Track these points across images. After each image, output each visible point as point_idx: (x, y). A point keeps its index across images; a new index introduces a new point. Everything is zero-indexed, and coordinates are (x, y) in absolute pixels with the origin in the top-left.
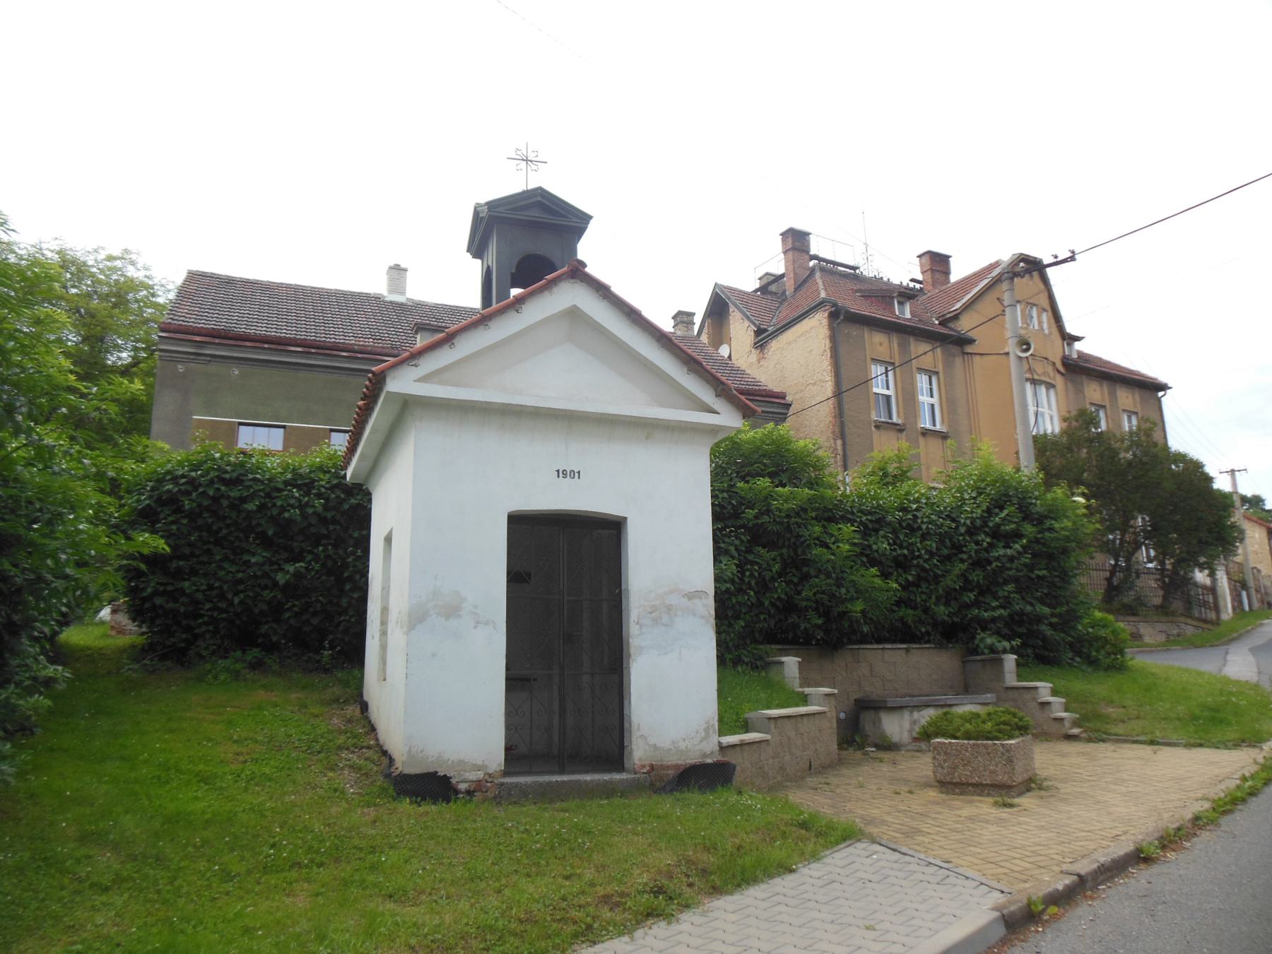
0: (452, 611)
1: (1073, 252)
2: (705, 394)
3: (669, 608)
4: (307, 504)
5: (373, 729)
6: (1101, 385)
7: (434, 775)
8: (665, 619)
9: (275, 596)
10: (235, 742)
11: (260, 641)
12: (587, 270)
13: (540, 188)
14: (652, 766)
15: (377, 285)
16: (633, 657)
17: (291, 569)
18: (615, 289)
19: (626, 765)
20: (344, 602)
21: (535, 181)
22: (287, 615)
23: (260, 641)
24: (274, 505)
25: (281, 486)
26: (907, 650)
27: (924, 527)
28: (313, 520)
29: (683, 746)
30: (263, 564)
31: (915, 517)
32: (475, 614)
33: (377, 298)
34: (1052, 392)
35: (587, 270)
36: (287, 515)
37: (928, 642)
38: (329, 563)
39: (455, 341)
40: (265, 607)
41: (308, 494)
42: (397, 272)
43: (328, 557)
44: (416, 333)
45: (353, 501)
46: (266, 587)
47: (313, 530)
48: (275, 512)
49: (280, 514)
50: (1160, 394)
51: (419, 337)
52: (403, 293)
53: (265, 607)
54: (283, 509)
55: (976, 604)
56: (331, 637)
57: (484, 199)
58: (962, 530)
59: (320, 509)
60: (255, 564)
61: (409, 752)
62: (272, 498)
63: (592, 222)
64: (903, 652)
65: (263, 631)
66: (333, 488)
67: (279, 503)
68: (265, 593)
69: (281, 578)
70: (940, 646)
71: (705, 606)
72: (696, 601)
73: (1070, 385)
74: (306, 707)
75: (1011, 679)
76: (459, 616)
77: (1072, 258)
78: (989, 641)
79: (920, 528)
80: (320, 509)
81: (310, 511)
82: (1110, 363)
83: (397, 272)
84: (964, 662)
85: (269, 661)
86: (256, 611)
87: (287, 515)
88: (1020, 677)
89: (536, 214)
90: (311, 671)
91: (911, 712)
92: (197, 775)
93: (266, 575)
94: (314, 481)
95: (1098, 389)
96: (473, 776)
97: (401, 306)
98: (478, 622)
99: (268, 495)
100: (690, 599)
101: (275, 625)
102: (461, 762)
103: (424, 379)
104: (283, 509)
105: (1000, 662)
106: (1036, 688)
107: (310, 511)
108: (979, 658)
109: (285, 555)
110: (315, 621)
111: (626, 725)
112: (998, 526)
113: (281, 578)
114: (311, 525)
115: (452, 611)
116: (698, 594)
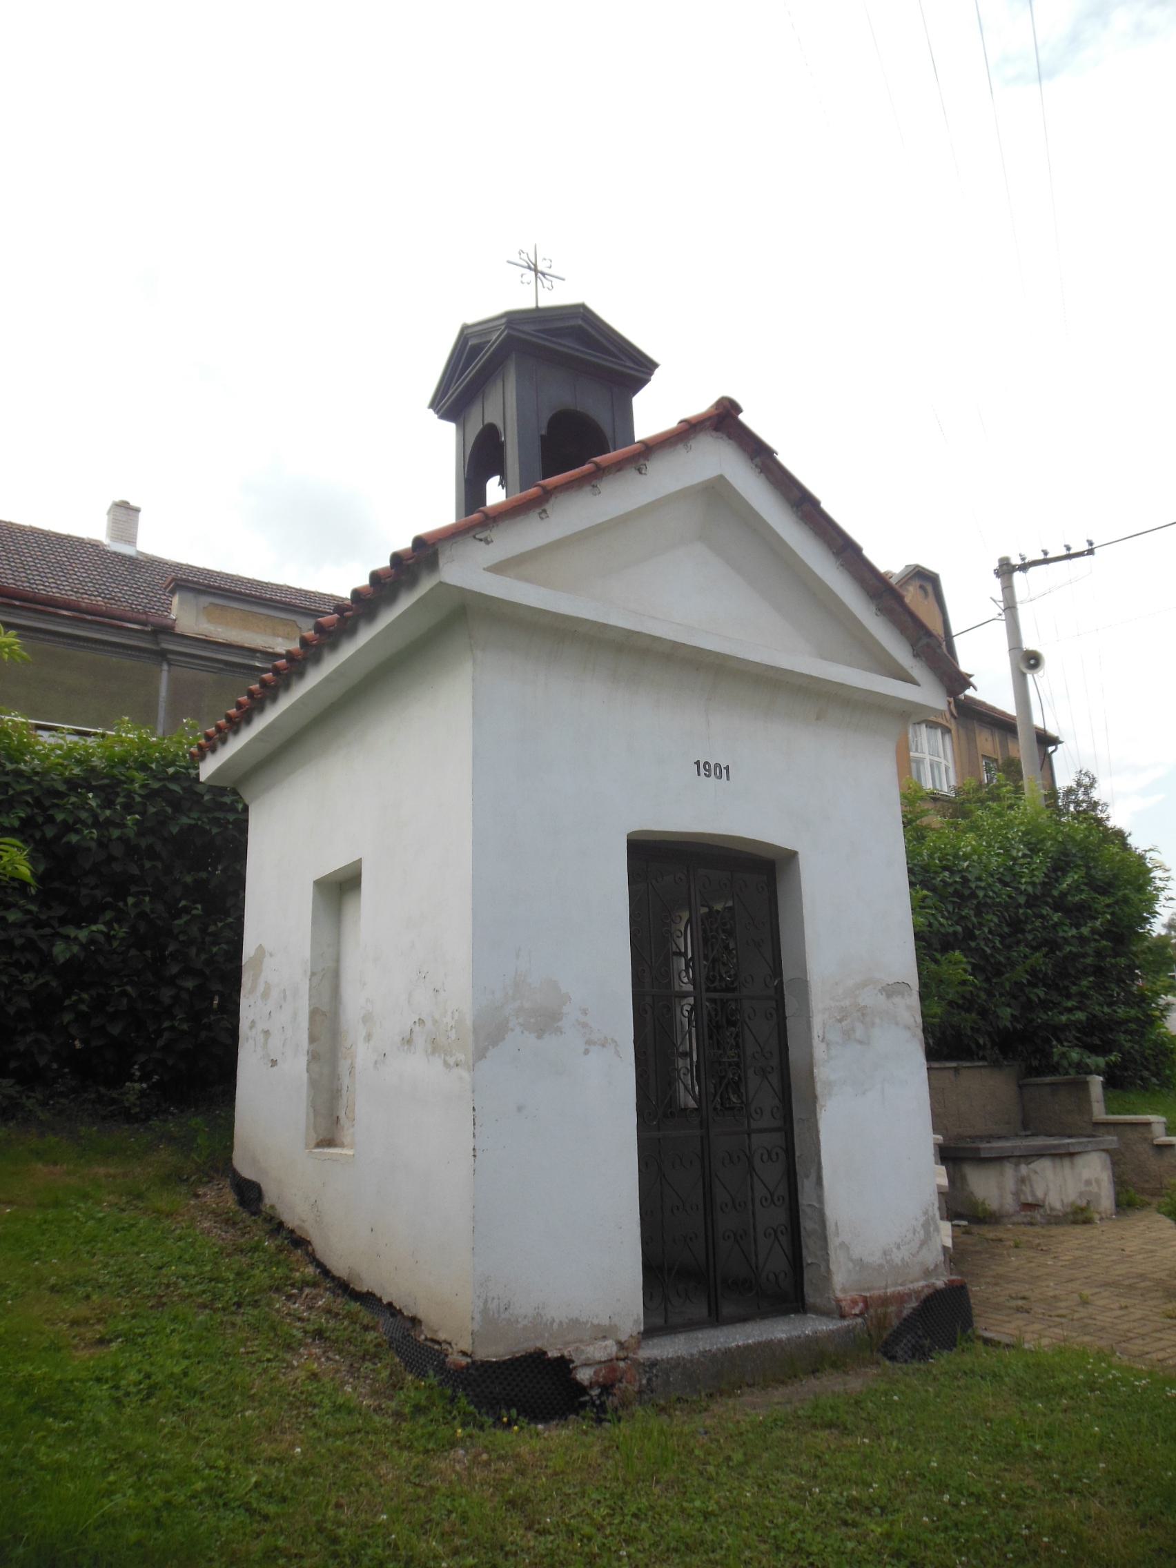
0: (546, 1021)
1: (1091, 543)
2: (900, 652)
3: (863, 1011)
4: (109, 823)
5: (299, 1242)
6: (993, 735)
7: (538, 1357)
8: (859, 1033)
9: (46, 984)
10: (53, 1289)
11: (13, 1065)
12: (741, 417)
13: (583, 307)
14: (865, 1300)
15: (92, 526)
16: (821, 1101)
17: (83, 935)
18: (783, 458)
19: (811, 1297)
20: (166, 994)
21: (552, 297)
22: (67, 1017)
23: (13, 1065)
24: (51, 820)
25: (62, 788)
26: (956, 1069)
27: (981, 894)
28: (117, 851)
29: (897, 1257)
30: (22, 925)
31: (965, 880)
32: (585, 1025)
33: (95, 546)
34: (947, 737)
35: (741, 417)
36: (74, 838)
37: (983, 1058)
38: (142, 927)
39: (548, 507)
40: (26, 1004)
41: (108, 803)
42: (125, 513)
43: (142, 915)
44: (173, 592)
45: (185, 820)
46: (28, 967)
47: (117, 867)
48: (50, 832)
49: (58, 838)
50: (1051, 749)
51: (176, 600)
52: (132, 541)
53: (26, 1004)
54: (68, 828)
55: (1045, 1005)
56: (142, 1058)
57: (471, 320)
58: (1022, 900)
59: (131, 832)
60: (14, 924)
61: (485, 1311)
62: (44, 809)
63: (657, 371)
64: (952, 1072)
65: (21, 1047)
66: (152, 795)
67: (60, 817)
68: (27, 977)
69: (61, 951)
70: (995, 1064)
71: (909, 1007)
72: (897, 1000)
73: (961, 731)
74: (139, 1196)
75: (1099, 1112)
76: (559, 1031)
77: (1090, 552)
78: (1075, 1055)
79: (973, 895)
80: (131, 832)
81: (116, 833)
82: (993, 709)
83: (125, 513)
84: (1020, 1087)
85: (29, 1104)
86: (11, 1010)
87: (74, 838)
88: (1109, 1111)
89: (568, 346)
90: (104, 1118)
91: (1017, 1165)
92: (22, 1393)
93: (30, 945)
94: (120, 782)
95: (990, 739)
96: (603, 1350)
97: (130, 558)
98: (589, 1042)
99: (38, 802)
100: (889, 996)
101: (43, 1037)
102: (575, 1323)
103: (498, 568)
104: (68, 828)
105: (1085, 1086)
106: (1148, 1124)
107: (116, 833)
108: (1048, 1079)
109: (60, 911)
110: (115, 1030)
111: (807, 1224)
112: (1063, 895)
113: (61, 951)
114: (111, 859)
115: (546, 1021)
116: (893, 990)
